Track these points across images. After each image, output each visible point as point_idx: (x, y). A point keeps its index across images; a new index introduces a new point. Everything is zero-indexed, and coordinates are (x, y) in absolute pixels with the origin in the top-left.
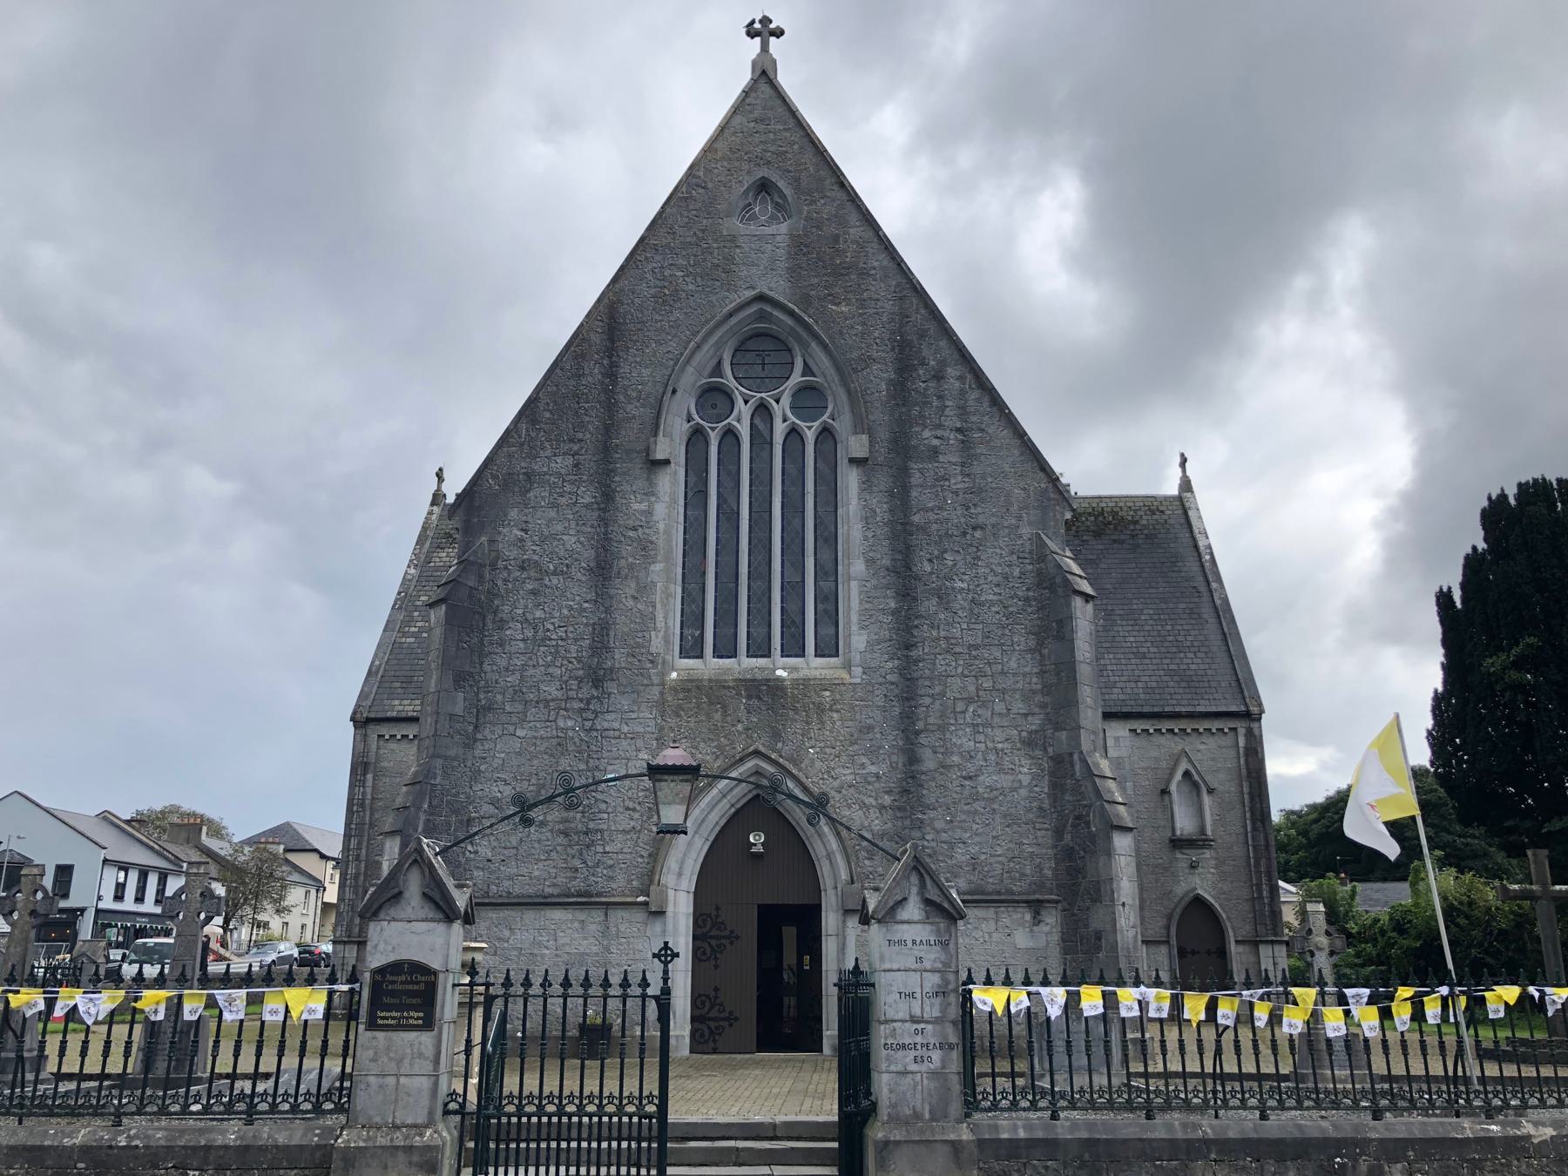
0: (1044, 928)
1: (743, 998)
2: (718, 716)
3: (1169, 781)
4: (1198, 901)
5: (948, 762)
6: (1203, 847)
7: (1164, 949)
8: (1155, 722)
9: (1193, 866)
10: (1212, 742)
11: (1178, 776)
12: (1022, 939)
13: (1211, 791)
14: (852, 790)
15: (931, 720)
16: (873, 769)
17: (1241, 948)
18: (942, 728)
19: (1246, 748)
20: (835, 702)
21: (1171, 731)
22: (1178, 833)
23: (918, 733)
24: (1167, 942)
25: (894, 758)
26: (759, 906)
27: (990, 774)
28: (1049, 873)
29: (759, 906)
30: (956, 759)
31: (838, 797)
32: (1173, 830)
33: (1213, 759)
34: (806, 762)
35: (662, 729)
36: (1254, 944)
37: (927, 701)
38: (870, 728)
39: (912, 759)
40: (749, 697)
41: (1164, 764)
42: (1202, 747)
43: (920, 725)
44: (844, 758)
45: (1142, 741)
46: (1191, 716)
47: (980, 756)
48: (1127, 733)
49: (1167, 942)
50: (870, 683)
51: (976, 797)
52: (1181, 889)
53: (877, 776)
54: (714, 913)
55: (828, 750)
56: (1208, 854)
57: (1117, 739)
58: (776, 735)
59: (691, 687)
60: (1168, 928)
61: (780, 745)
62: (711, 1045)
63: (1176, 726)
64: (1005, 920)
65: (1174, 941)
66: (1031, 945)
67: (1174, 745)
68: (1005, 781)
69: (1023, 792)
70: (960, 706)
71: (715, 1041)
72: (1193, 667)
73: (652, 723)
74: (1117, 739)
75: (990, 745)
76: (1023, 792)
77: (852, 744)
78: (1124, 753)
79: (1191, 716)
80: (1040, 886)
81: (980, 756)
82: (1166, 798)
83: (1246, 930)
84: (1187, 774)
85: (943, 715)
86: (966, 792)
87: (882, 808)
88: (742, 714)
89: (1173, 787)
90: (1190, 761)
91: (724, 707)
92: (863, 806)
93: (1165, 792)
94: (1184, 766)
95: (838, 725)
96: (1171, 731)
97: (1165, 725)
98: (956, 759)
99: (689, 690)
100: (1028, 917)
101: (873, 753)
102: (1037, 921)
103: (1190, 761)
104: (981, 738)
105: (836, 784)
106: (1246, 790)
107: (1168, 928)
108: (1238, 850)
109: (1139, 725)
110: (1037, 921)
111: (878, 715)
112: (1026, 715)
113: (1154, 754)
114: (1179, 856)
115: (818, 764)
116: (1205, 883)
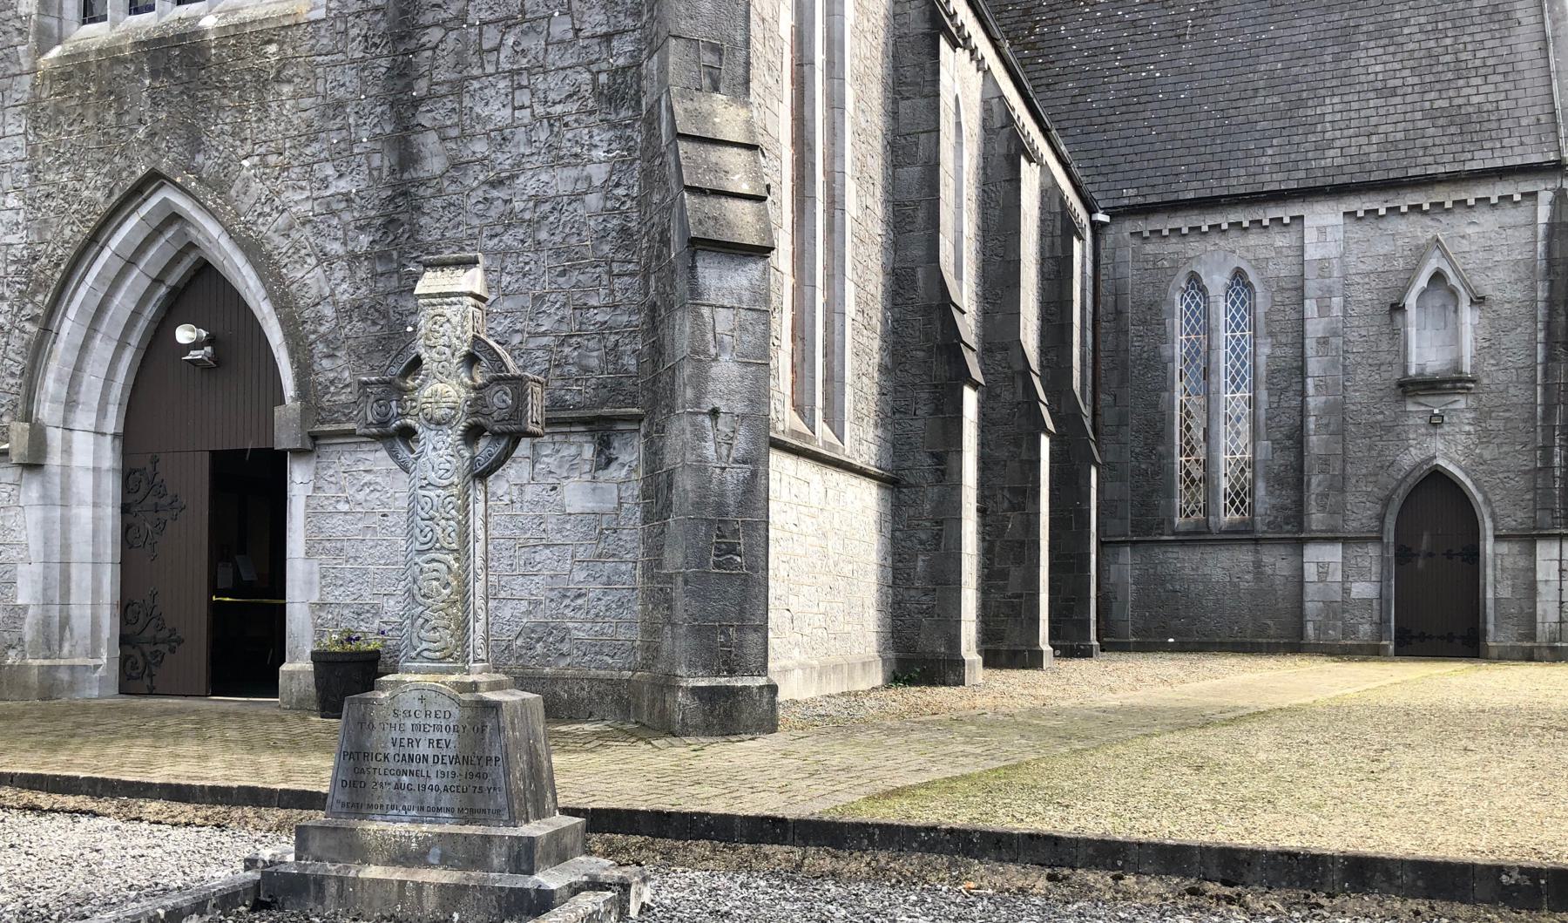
0: (616, 472)
1: (189, 610)
2: (110, 117)
3: (1405, 290)
4: (1437, 479)
5: (466, 155)
6: (1454, 391)
7: (1373, 550)
8: (1390, 196)
9: (1435, 422)
10: (1487, 221)
11: (1422, 281)
12: (577, 496)
13: (1478, 301)
14: (308, 229)
15: (440, 75)
16: (343, 185)
17: (1504, 548)
18: (458, 88)
19: (1551, 226)
20: (284, 62)
21: (1415, 209)
22: (1413, 371)
23: (416, 103)
24: (1380, 539)
25: (376, 160)
26: (215, 456)
27: (536, 172)
28: (630, 362)
29: (213, 454)
30: (480, 147)
31: (285, 244)
32: (1405, 368)
33: (1489, 249)
34: (238, 184)
35: (34, 151)
36: (1528, 539)
37: (435, 34)
38: (340, 105)
39: (407, 157)
40: (154, 74)
41: (1400, 264)
42: (1470, 230)
43: (420, 89)
44: (296, 172)
45: (1358, 231)
46: (1454, 179)
47: (521, 135)
48: (1340, 219)
49: (1380, 539)
50: (341, 16)
51: (510, 220)
52: (1411, 457)
53: (347, 198)
54: (149, 468)
55: (272, 159)
56: (1461, 402)
57: (1322, 230)
58: (195, 143)
59: (76, 70)
60: (1381, 519)
61: (200, 158)
62: (147, 681)
63: (1424, 199)
64: (548, 461)
65: (1390, 537)
66: (590, 505)
67: (1417, 230)
68: (561, 181)
69: (594, 200)
70: (491, 37)
71: (151, 676)
72: (1475, 100)
73: (21, 142)
74: (1322, 230)
75: (540, 110)
76: (594, 200)
77: (310, 142)
78: (1333, 250)
79: (1454, 179)
80: (613, 390)
81: (521, 135)
82: (1398, 318)
83: (1516, 518)
84: (1438, 277)
85: (460, 62)
86: (494, 213)
87: (354, 257)
88: (144, 107)
89: (1411, 301)
90: (1445, 254)
91: (119, 99)
92: (325, 258)
93: (1397, 308)
94: (1433, 263)
95: (290, 107)
96: (1415, 209)
97: (1405, 200)
98: (480, 147)
99: (70, 76)
100: (588, 451)
101: (342, 156)
102: (605, 459)
103: (1445, 254)
104: (523, 97)
105: (282, 221)
106: (1542, 294)
107: (1381, 519)
108: (1517, 394)
109: (1360, 204)
110: (605, 459)
111: (350, 77)
112: (608, 37)
113: (1384, 248)
114: (1411, 407)
115: (256, 187)
116: (1450, 451)
